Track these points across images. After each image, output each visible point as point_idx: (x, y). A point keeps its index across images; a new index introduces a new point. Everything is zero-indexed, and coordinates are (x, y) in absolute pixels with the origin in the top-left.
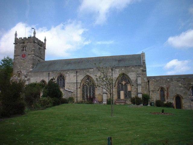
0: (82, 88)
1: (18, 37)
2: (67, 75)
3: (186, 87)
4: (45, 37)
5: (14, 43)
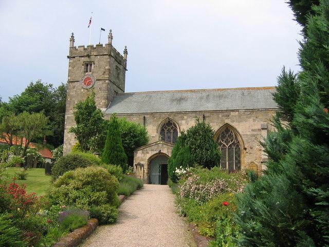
2: (184, 122)
4: (111, 31)
5: (68, 57)
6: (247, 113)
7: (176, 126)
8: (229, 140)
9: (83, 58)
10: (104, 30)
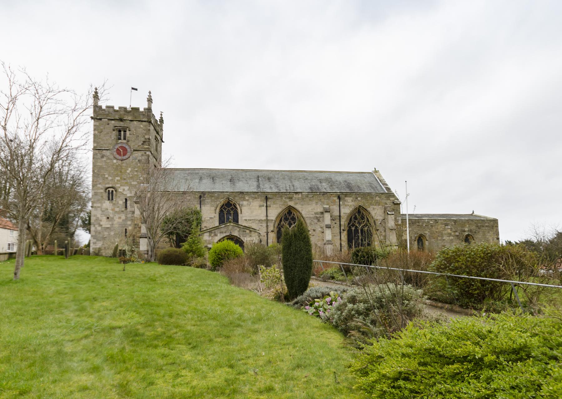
0: (276, 231)
1: (103, 104)
2: (245, 203)
3: (457, 236)
4: (150, 93)
5: (92, 118)
6: (310, 196)
7: (236, 208)
8: (292, 222)
9: (113, 122)
10: (136, 90)
